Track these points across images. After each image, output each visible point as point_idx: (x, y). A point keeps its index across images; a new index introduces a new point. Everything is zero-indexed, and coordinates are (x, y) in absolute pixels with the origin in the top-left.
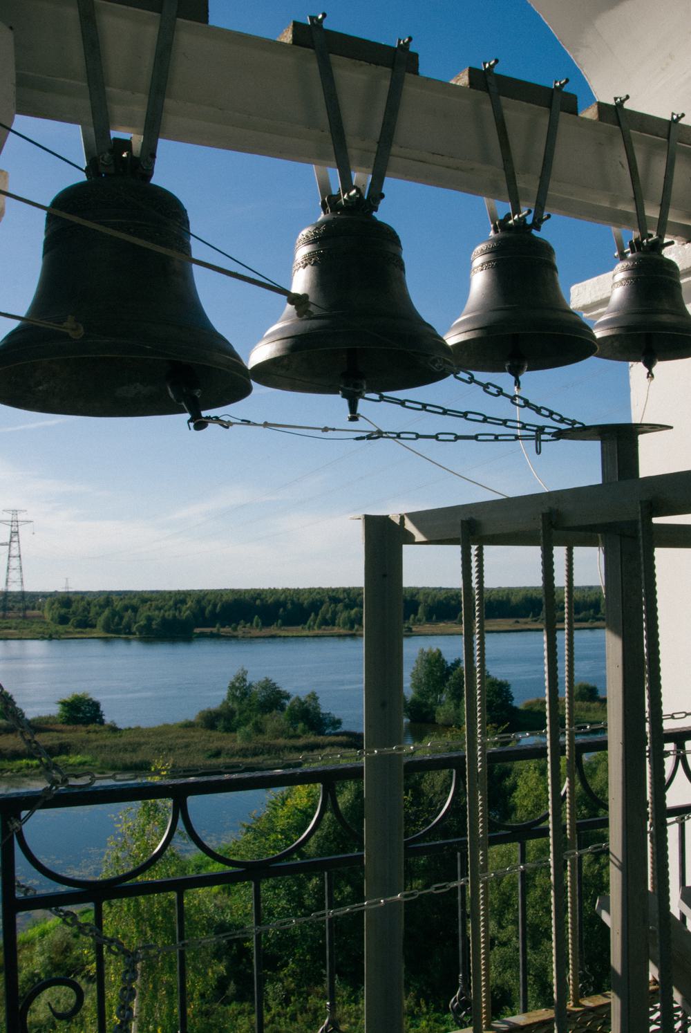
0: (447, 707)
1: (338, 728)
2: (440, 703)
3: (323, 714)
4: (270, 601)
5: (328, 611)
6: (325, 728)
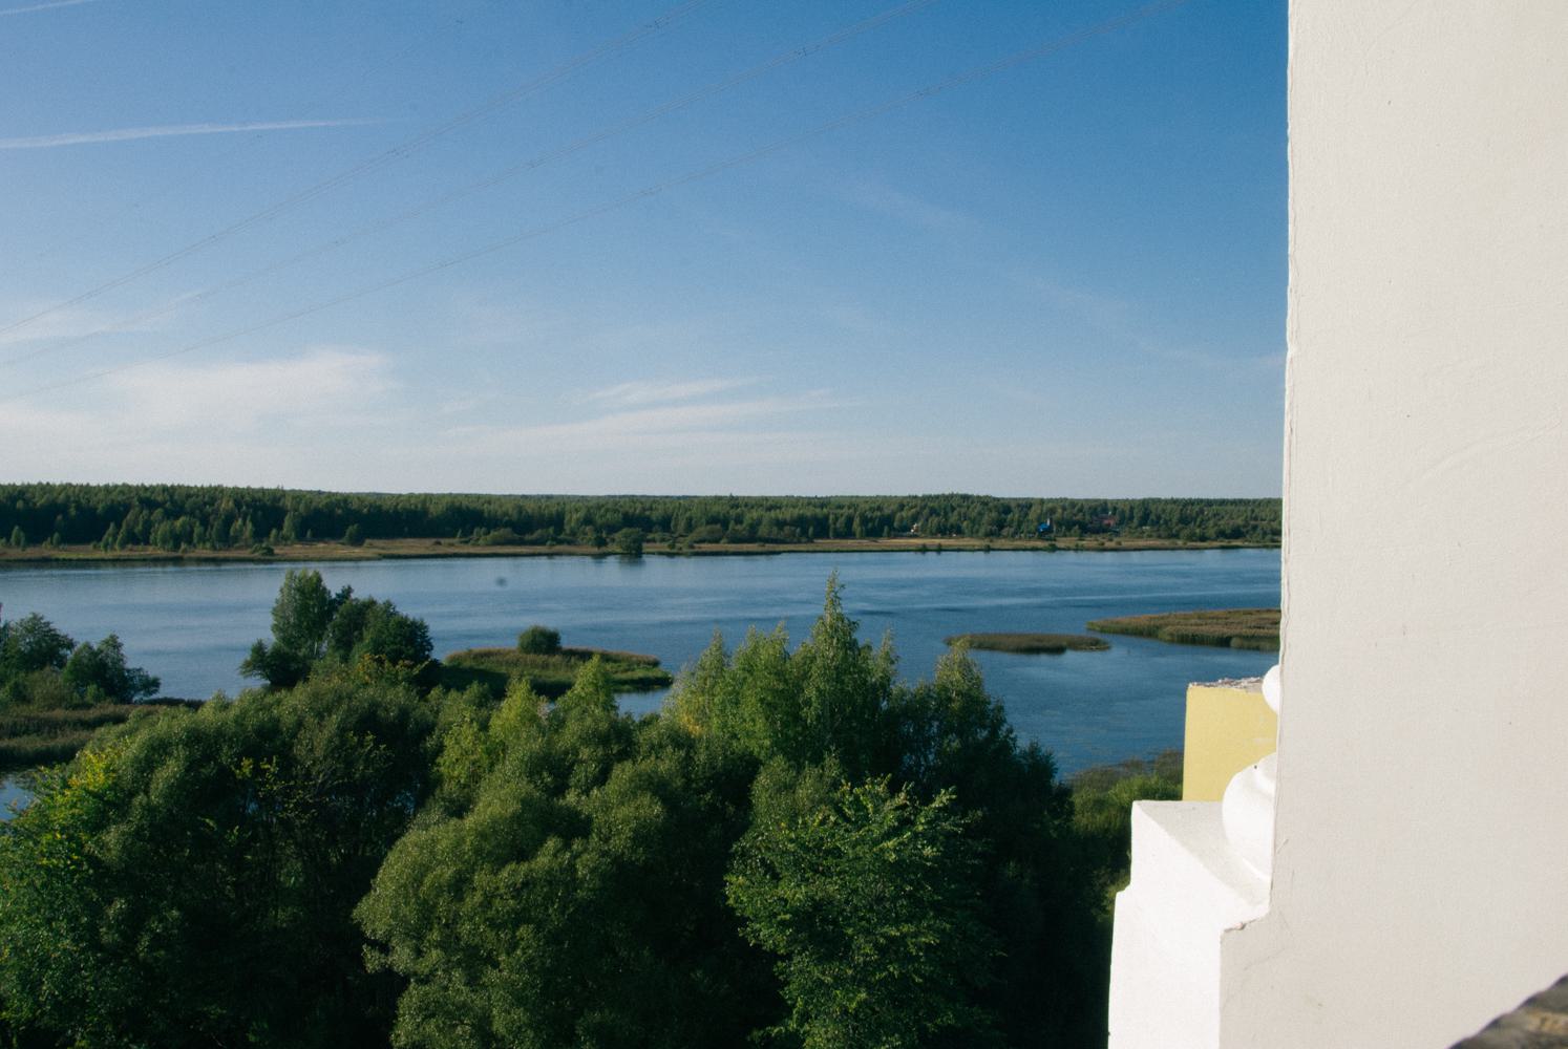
0: (328, 660)
1: (155, 691)
2: (318, 655)
3: (128, 671)
4: (40, 502)
5: (136, 522)
6: (132, 692)
